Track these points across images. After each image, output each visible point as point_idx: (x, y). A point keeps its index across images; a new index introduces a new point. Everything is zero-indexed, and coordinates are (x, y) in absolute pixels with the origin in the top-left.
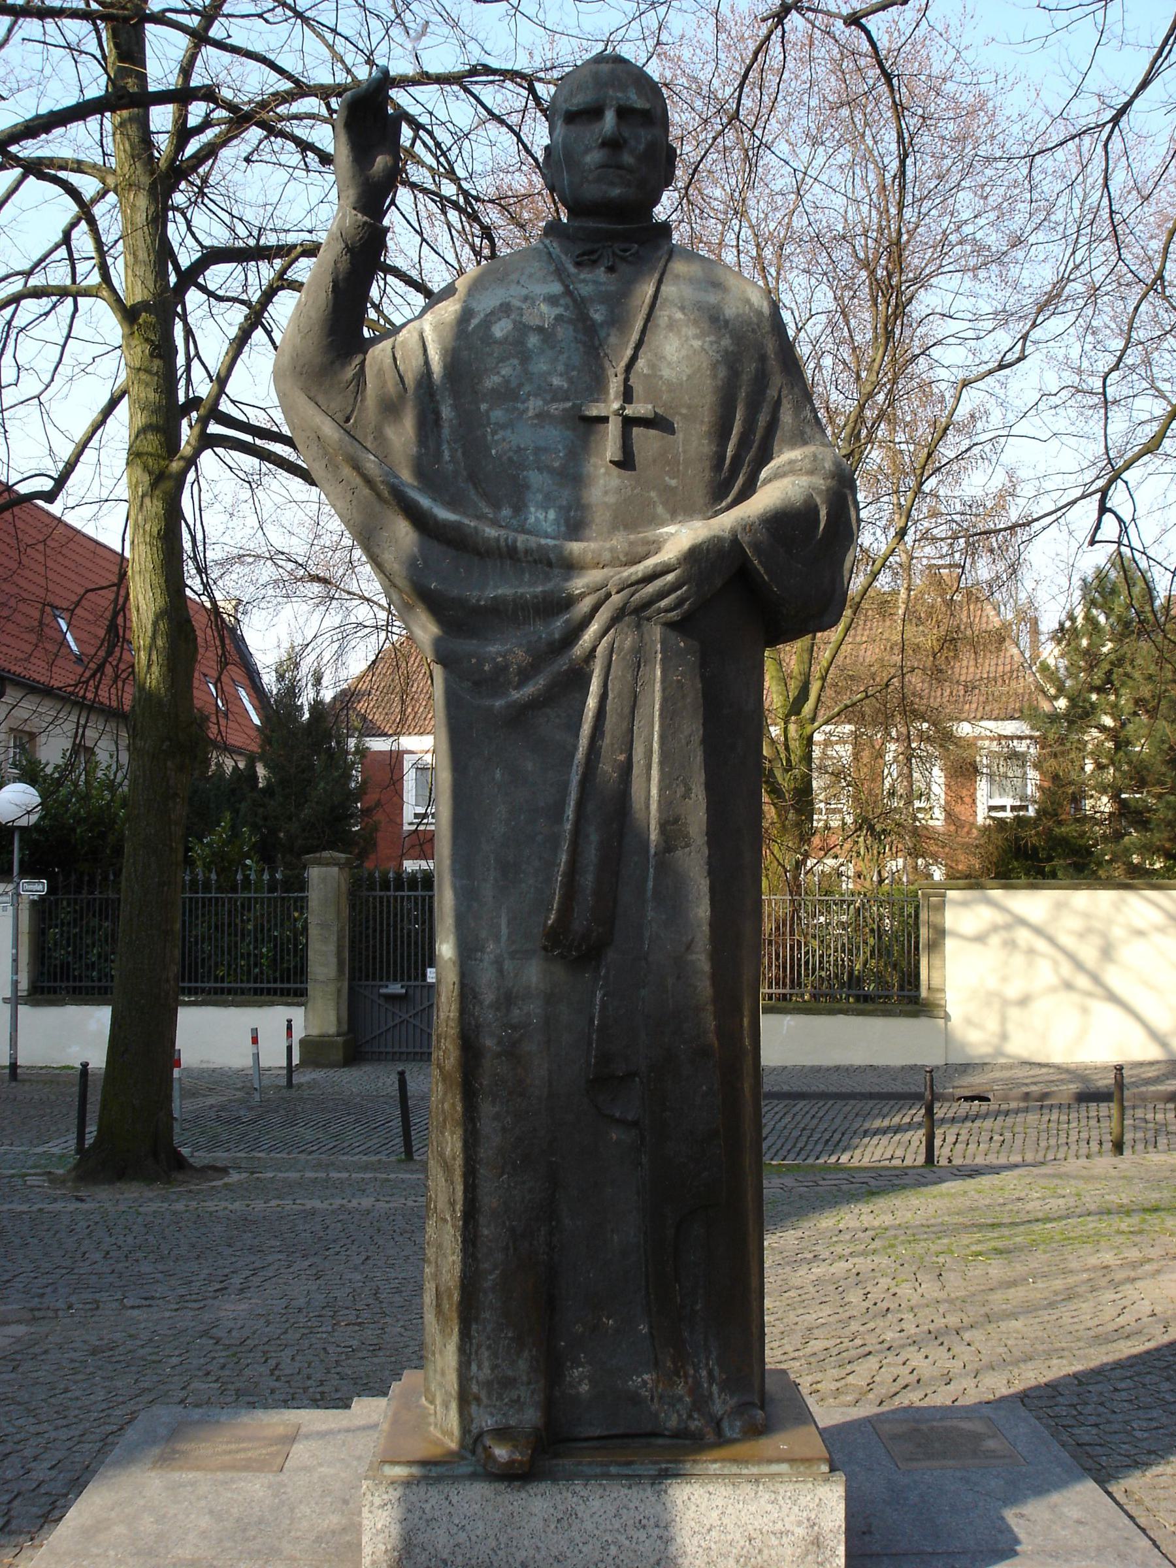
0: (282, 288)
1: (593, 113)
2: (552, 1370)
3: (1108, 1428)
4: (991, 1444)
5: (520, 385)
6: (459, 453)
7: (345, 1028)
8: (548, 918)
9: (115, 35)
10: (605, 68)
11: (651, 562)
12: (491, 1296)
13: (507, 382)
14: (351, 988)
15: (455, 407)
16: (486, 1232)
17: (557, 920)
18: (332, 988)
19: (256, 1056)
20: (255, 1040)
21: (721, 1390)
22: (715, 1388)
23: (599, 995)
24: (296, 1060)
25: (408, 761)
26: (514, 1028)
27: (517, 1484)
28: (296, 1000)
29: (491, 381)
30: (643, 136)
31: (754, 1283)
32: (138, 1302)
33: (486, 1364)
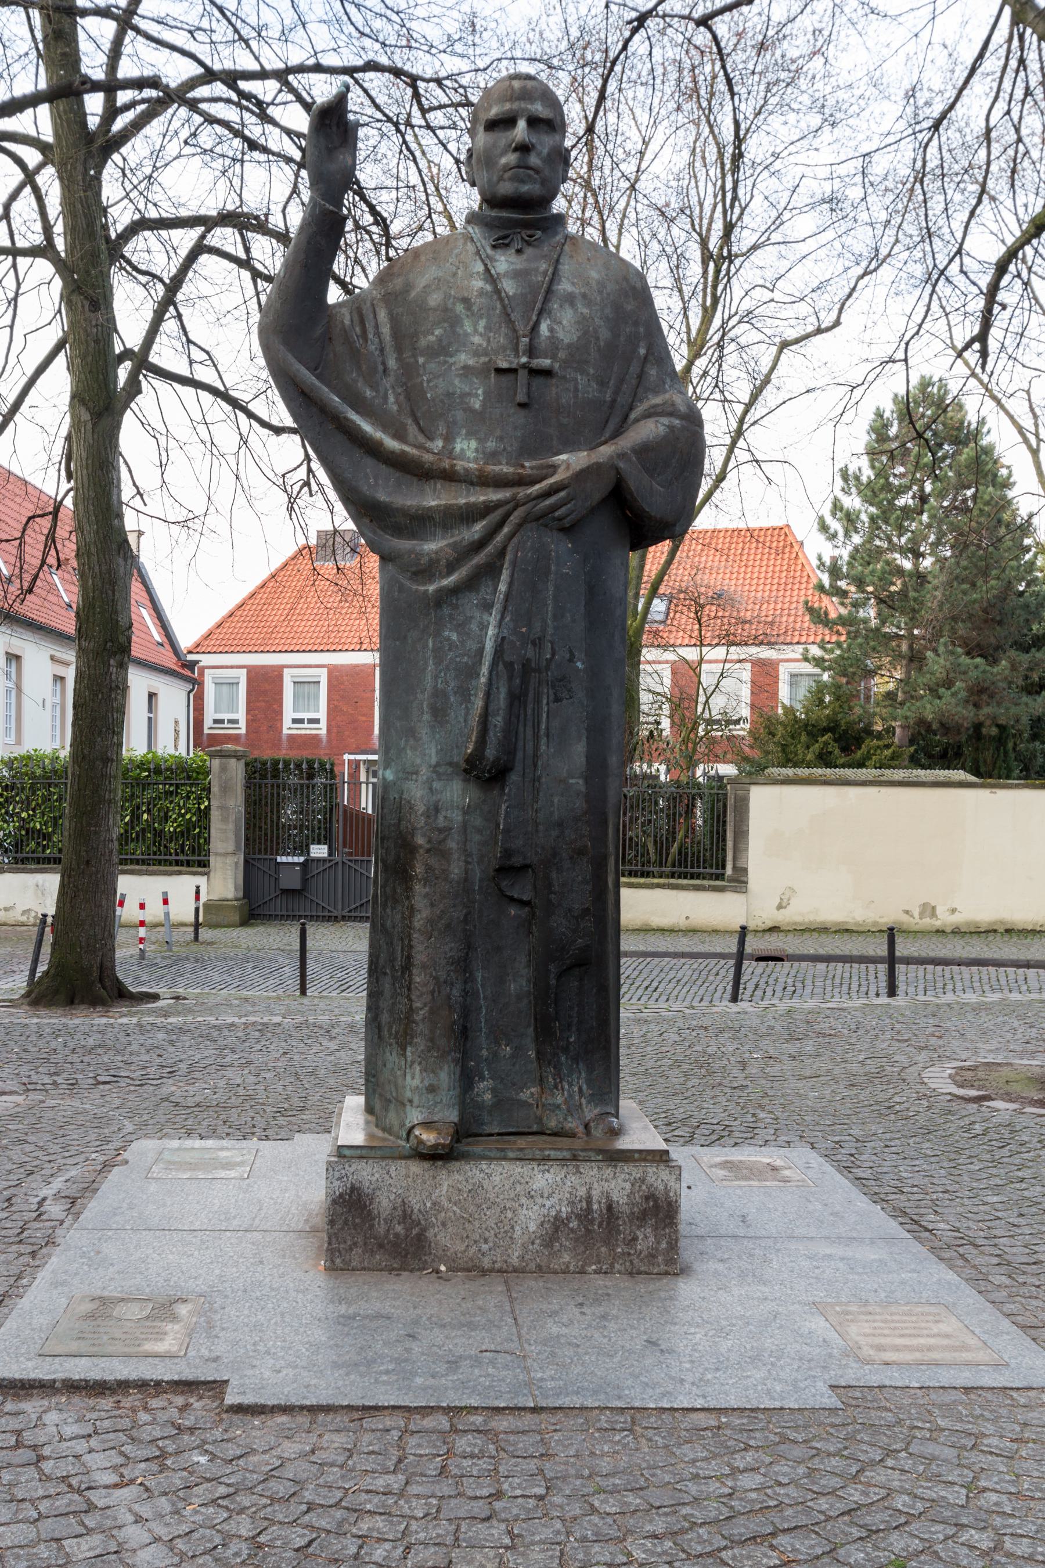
1: (506, 122)
2: (467, 1080)
3: (879, 1170)
5: (450, 344)
6: (402, 398)
7: (241, 894)
8: (467, 748)
9: (47, 19)
10: (516, 84)
12: (421, 1026)
13: (440, 340)
14: (246, 861)
15: (399, 359)
16: (418, 980)
17: (475, 749)
20: (166, 902)
21: (589, 1102)
22: (584, 1101)
23: (504, 807)
24: (201, 919)
26: (440, 830)
27: (440, 1163)
28: (200, 869)
30: (545, 142)
31: (613, 1034)
32: (108, 1079)
33: (417, 1076)
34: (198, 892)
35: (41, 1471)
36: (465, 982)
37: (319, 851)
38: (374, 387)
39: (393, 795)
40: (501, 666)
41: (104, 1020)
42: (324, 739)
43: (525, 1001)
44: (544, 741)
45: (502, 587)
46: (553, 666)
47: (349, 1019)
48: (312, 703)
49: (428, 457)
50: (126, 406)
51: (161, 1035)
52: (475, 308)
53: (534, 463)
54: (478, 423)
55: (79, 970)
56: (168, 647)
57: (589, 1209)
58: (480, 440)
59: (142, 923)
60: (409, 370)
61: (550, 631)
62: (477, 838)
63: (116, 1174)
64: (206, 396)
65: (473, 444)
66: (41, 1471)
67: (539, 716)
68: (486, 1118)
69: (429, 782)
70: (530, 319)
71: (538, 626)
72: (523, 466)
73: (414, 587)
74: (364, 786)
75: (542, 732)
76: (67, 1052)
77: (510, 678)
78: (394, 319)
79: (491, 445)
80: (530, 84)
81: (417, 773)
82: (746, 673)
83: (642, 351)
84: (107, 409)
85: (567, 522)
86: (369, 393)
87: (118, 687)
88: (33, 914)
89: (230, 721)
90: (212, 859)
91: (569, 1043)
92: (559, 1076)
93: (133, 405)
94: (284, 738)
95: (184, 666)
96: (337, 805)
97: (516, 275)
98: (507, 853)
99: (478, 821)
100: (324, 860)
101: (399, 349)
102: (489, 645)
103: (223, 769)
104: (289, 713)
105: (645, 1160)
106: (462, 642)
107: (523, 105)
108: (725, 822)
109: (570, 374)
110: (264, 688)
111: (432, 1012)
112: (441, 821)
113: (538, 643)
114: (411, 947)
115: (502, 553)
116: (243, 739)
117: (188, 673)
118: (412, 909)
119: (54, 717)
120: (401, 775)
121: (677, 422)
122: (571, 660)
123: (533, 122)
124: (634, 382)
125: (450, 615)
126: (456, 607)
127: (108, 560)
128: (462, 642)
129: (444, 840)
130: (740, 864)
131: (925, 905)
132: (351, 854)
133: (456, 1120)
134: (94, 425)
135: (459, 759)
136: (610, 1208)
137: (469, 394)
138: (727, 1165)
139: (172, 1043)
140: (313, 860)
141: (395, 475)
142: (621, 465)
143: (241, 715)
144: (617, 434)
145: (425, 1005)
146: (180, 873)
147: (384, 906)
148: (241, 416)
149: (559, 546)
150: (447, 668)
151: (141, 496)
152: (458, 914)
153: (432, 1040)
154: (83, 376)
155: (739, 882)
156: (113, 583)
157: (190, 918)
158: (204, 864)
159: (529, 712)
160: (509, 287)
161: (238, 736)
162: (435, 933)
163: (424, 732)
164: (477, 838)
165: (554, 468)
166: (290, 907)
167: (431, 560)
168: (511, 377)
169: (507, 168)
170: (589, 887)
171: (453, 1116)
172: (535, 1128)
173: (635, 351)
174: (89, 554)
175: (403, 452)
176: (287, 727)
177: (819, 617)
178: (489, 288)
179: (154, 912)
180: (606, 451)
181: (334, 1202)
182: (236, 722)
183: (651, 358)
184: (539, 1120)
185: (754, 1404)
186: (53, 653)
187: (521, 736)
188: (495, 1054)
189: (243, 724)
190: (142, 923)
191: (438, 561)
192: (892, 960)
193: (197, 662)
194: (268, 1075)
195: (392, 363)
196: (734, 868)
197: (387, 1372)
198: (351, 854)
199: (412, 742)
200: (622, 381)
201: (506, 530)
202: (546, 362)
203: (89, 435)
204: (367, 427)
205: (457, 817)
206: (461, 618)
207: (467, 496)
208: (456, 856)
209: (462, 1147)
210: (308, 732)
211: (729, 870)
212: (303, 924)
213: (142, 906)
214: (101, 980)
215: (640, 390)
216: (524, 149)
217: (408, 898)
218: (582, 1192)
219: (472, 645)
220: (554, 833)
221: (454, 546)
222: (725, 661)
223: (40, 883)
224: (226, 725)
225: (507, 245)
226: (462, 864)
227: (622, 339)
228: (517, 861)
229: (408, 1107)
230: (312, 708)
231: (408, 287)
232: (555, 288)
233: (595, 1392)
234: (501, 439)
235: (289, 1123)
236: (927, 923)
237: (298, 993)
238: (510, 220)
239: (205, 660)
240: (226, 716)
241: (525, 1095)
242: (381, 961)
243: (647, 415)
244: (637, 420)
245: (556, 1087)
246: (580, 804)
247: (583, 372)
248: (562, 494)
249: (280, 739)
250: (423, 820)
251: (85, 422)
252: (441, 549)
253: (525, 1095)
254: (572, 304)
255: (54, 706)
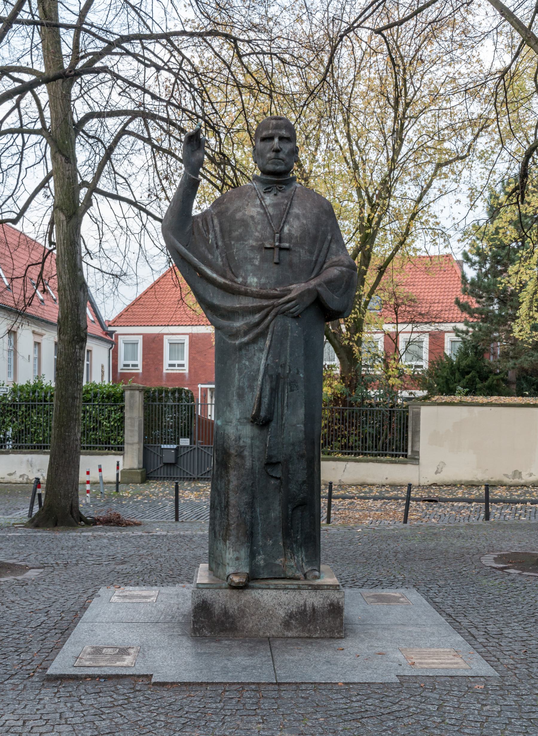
0: (124, 135)
2: (252, 555)
4: (402, 599)
6: (224, 259)
7: (141, 466)
11: (289, 297)
13: (241, 234)
15: (223, 241)
18: (136, 447)
19: (101, 477)
20: (100, 470)
21: (306, 565)
23: (269, 437)
24: (120, 480)
25: (166, 341)
26: (241, 447)
28: (119, 452)
29: (236, 234)
30: (287, 147)
34: (118, 465)
35: (81, 703)
36: (252, 513)
37: (185, 442)
38: (212, 254)
39: (221, 431)
40: (267, 376)
41: (74, 534)
42: (187, 376)
43: (278, 521)
44: (286, 408)
45: (268, 343)
46: (290, 376)
47: (202, 533)
48: (180, 355)
49: (235, 285)
50: (85, 211)
51: (105, 541)
52: (256, 220)
53: (282, 288)
54: (257, 271)
55: (58, 508)
56: (98, 323)
57: (305, 610)
58: (258, 278)
59: (88, 482)
60: (228, 247)
61: (288, 361)
62: (257, 450)
63: (95, 600)
64: (125, 205)
65: (255, 280)
66: (81, 703)
67: (284, 398)
68: (262, 572)
69: (236, 426)
70: (280, 226)
71: (283, 359)
72: (276, 290)
73: (230, 342)
74: (209, 406)
75: (285, 404)
76: (59, 549)
77: (271, 382)
78: (221, 223)
79: (263, 280)
80: (280, 122)
81: (231, 422)
82: (426, 339)
83: (329, 237)
84: (74, 213)
85: (295, 314)
86: (210, 257)
87: (80, 359)
88: (26, 477)
89: (133, 365)
90: (126, 446)
91: (297, 539)
92: (293, 553)
93: (88, 211)
94: (164, 375)
95: (107, 334)
96: (195, 415)
97: (275, 205)
98: (270, 457)
99: (258, 443)
100: (188, 447)
101: (223, 237)
102: (262, 368)
103: (132, 396)
104: (167, 361)
105: (329, 589)
106: (251, 366)
107: (277, 131)
108: (407, 427)
109: (297, 249)
110: (153, 346)
111: (237, 525)
112: (241, 443)
113: (283, 366)
114: (228, 497)
115: (268, 327)
116: (140, 376)
117: (108, 338)
118: (229, 481)
119: (35, 365)
120: (224, 423)
121: (344, 269)
122: (298, 373)
123: (281, 138)
124: (326, 251)
125: (245, 354)
126: (248, 351)
127: (75, 293)
128: (251, 366)
129: (243, 451)
130: (415, 449)
131: (516, 471)
132: (202, 444)
133: (248, 572)
134: (68, 223)
135: (249, 416)
136: (314, 609)
137: (254, 258)
138: (375, 596)
139: (111, 544)
140: (181, 447)
141: (221, 292)
142: (319, 289)
143: (139, 362)
144: (318, 275)
145: (235, 522)
146: (107, 454)
147: (217, 480)
148: (144, 215)
149: (291, 324)
150: (244, 377)
151: (90, 254)
152: (249, 483)
153: (238, 537)
154: (61, 197)
155: (415, 459)
156: (78, 305)
157: (114, 479)
158: (121, 449)
159: (280, 396)
160: (270, 210)
161: (137, 375)
162: (239, 492)
163: (234, 405)
164: (257, 450)
165: (290, 291)
166: (169, 472)
167: (237, 330)
168: (271, 251)
169: (270, 159)
170: (306, 471)
171: (247, 570)
172: (283, 576)
173: (326, 238)
174: (65, 290)
175: (225, 283)
176: (166, 369)
177: (464, 307)
178: (262, 211)
179: (94, 476)
180: (313, 283)
181: (195, 608)
182: (136, 365)
183: (333, 240)
184: (284, 572)
185: (364, 681)
186: (33, 329)
187: (276, 406)
188: (265, 544)
189: (140, 367)
190: (88, 482)
191: (240, 330)
192: (487, 501)
193: (114, 332)
194: (161, 560)
195: (220, 243)
196: (412, 451)
197: (217, 671)
198: (202, 444)
199: (229, 409)
200: (320, 251)
201: (269, 318)
202: (286, 245)
203: (65, 227)
204: (209, 272)
205: (249, 441)
206: (250, 355)
207: (253, 303)
208: (248, 458)
209: (251, 584)
210: (178, 372)
211: (409, 453)
212: (177, 483)
213: (88, 473)
214: (71, 513)
215: (329, 254)
216: (277, 151)
217: (227, 476)
218: (302, 602)
219: (255, 367)
220: (291, 448)
221: (246, 324)
222: (412, 332)
223: (30, 459)
224: (131, 368)
225: (270, 192)
226: (251, 462)
227: (320, 233)
228: (274, 460)
229: (227, 567)
230: (180, 357)
231: (227, 209)
232: (290, 211)
233: (301, 677)
234: (267, 278)
235: (173, 581)
236: (517, 480)
237: (174, 520)
238: (271, 181)
239: (119, 330)
240: (131, 363)
241: (278, 562)
242: (216, 504)
243: (331, 266)
244: (327, 268)
245: (291, 558)
246: (301, 435)
247: (303, 248)
248: (293, 302)
249: (162, 376)
250: (234, 442)
251: (63, 221)
252: (242, 326)
253: (278, 562)
254: (298, 219)
255: (35, 359)
